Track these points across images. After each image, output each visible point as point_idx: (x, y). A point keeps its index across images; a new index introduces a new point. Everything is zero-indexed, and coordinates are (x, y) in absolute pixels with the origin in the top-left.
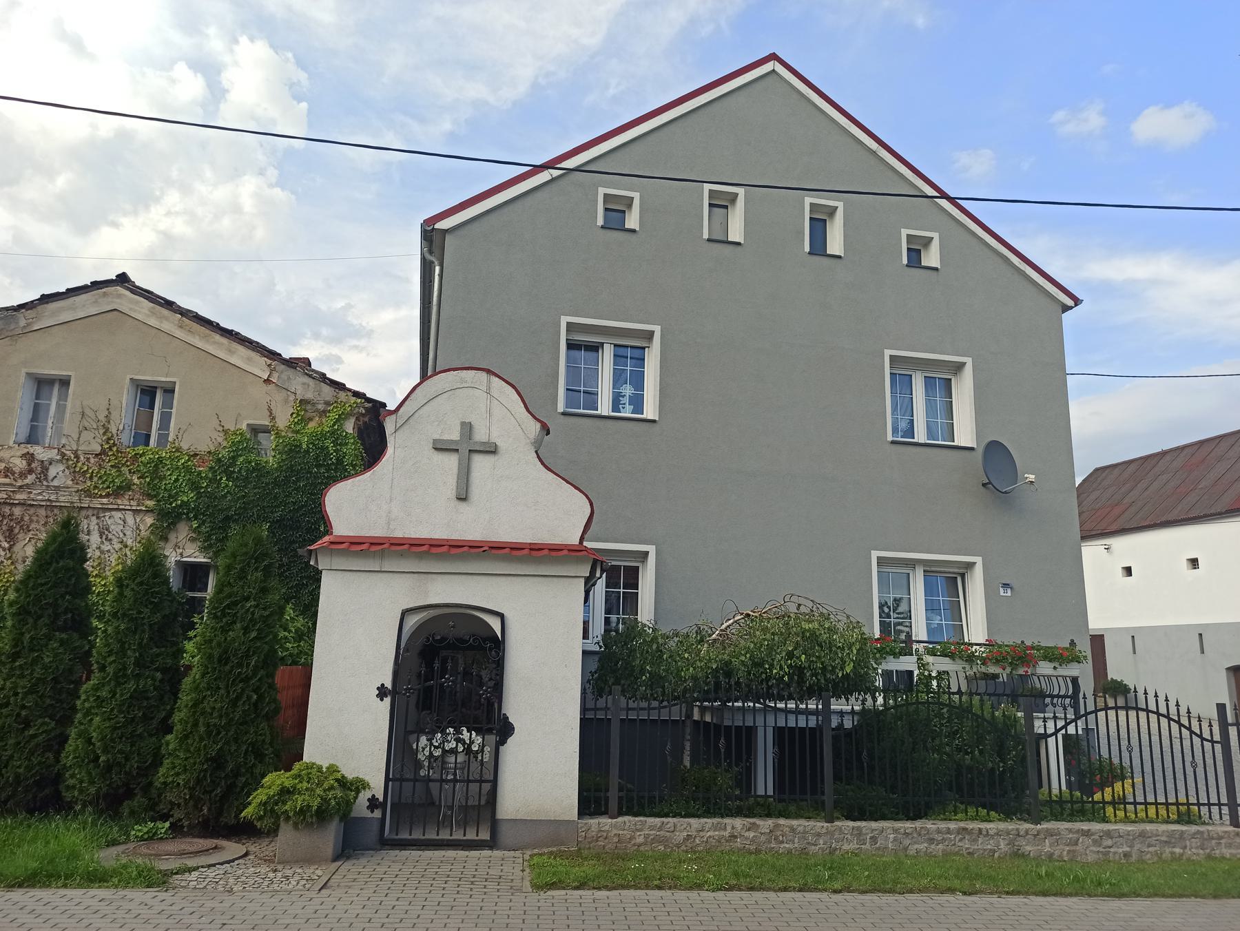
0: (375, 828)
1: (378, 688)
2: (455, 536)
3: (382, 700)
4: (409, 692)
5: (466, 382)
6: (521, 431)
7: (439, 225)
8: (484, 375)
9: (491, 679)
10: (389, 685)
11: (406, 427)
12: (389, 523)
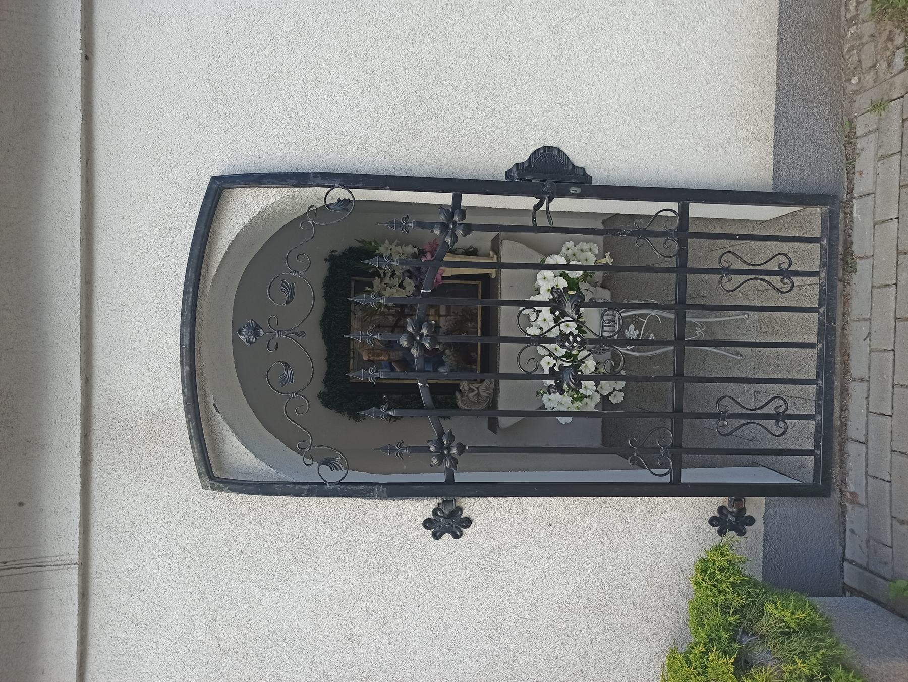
0: (788, 506)
1: (437, 536)
4: (449, 449)
9: (401, 285)
10: (426, 507)
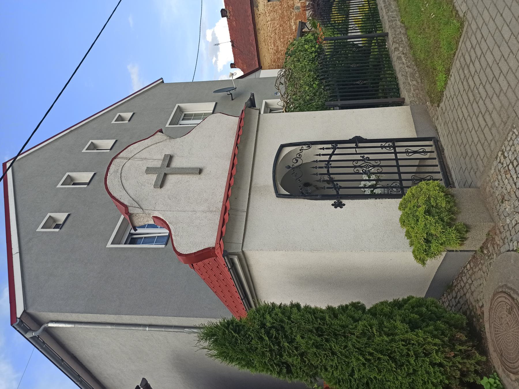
2: (226, 174)
3: (344, 205)
5: (118, 170)
6: (160, 143)
7: (19, 315)
8: (116, 161)
11: (140, 203)
12: (211, 212)
